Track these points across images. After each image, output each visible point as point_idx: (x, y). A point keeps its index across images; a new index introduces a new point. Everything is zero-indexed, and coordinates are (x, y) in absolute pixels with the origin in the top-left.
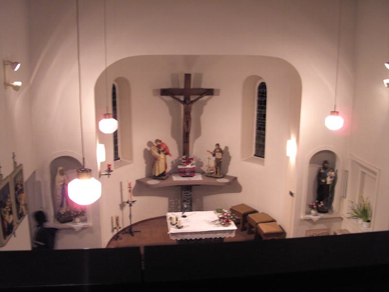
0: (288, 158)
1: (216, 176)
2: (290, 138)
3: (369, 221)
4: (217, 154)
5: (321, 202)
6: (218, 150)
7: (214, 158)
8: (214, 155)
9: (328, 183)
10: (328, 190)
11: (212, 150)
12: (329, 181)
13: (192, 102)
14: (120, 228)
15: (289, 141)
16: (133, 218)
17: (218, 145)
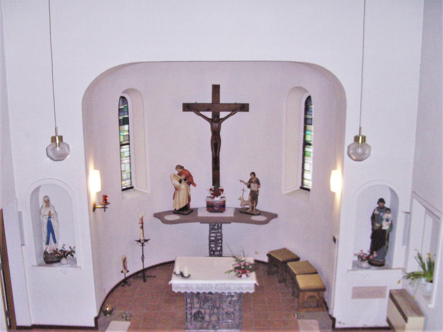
0: (333, 194)
1: (252, 213)
2: (335, 168)
3: (431, 282)
4: (252, 185)
5: (375, 252)
6: (254, 180)
7: (248, 191)
8: (249, 187)
9: (384, 228)
10: (385, 237)
11: (247, 181)
12: (385, 226)
13: (224, 119)
14: (128, 271)
15: (334, 172)
16: (294, 263)
17: (253, 174)
